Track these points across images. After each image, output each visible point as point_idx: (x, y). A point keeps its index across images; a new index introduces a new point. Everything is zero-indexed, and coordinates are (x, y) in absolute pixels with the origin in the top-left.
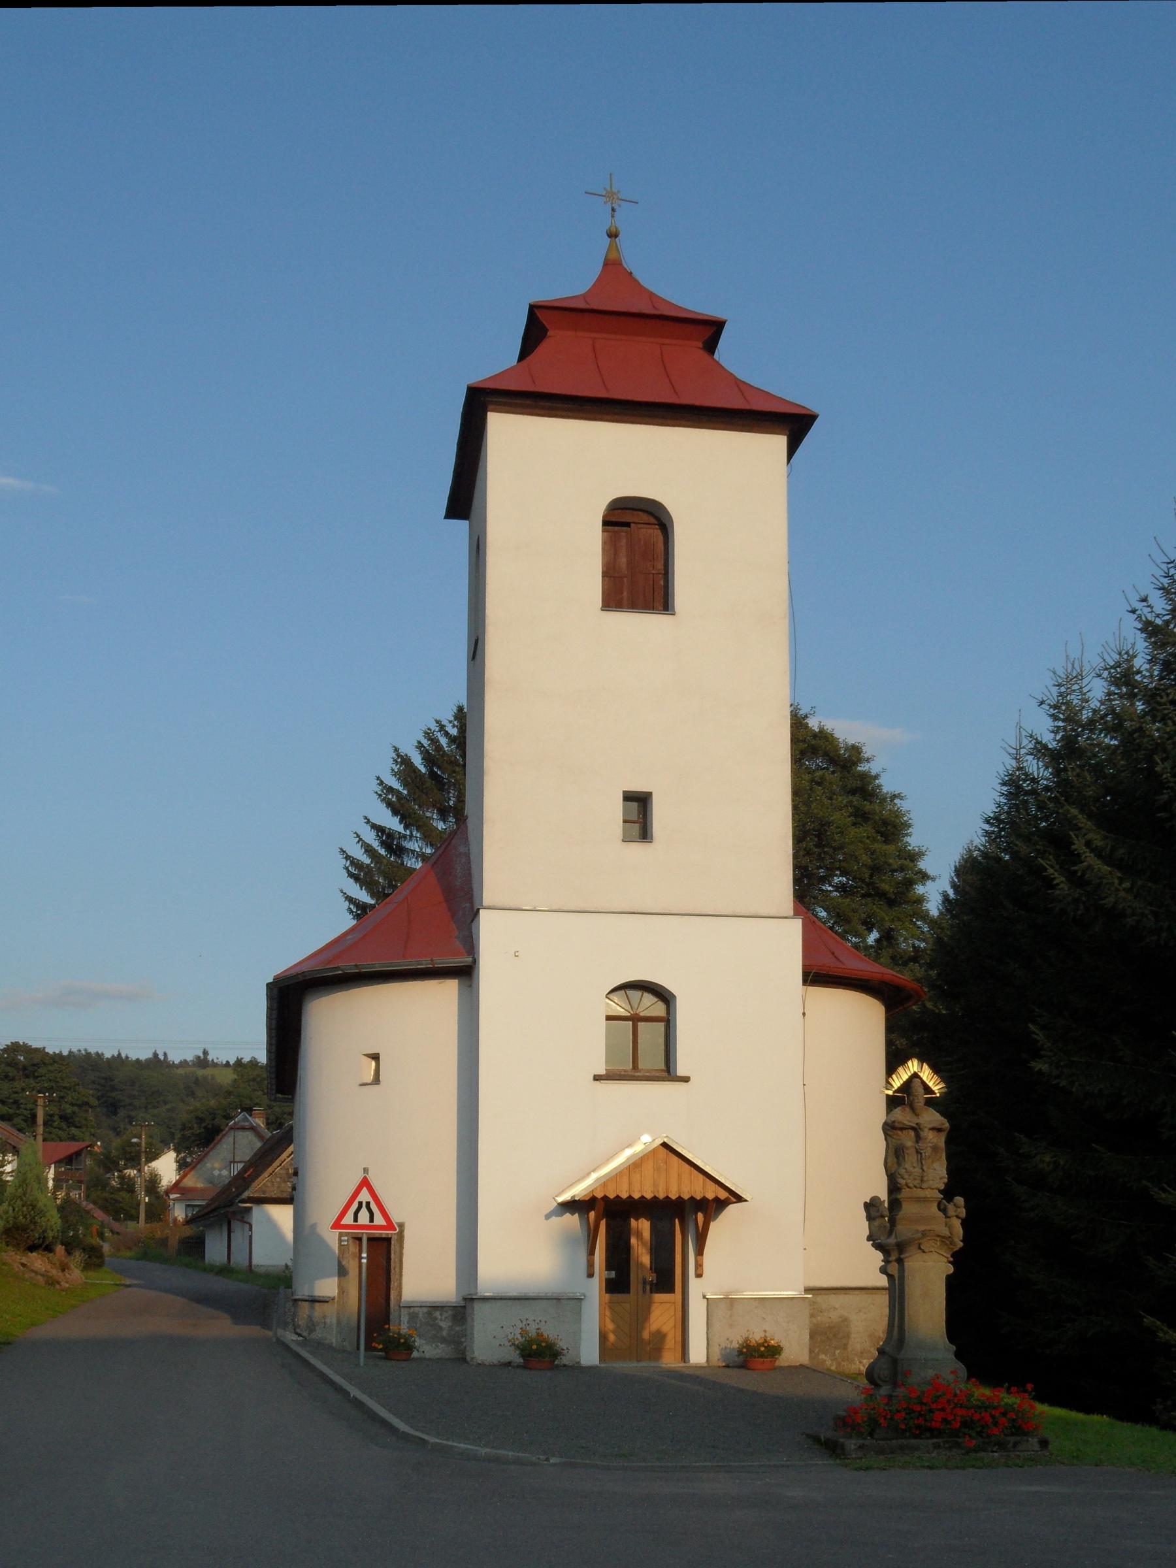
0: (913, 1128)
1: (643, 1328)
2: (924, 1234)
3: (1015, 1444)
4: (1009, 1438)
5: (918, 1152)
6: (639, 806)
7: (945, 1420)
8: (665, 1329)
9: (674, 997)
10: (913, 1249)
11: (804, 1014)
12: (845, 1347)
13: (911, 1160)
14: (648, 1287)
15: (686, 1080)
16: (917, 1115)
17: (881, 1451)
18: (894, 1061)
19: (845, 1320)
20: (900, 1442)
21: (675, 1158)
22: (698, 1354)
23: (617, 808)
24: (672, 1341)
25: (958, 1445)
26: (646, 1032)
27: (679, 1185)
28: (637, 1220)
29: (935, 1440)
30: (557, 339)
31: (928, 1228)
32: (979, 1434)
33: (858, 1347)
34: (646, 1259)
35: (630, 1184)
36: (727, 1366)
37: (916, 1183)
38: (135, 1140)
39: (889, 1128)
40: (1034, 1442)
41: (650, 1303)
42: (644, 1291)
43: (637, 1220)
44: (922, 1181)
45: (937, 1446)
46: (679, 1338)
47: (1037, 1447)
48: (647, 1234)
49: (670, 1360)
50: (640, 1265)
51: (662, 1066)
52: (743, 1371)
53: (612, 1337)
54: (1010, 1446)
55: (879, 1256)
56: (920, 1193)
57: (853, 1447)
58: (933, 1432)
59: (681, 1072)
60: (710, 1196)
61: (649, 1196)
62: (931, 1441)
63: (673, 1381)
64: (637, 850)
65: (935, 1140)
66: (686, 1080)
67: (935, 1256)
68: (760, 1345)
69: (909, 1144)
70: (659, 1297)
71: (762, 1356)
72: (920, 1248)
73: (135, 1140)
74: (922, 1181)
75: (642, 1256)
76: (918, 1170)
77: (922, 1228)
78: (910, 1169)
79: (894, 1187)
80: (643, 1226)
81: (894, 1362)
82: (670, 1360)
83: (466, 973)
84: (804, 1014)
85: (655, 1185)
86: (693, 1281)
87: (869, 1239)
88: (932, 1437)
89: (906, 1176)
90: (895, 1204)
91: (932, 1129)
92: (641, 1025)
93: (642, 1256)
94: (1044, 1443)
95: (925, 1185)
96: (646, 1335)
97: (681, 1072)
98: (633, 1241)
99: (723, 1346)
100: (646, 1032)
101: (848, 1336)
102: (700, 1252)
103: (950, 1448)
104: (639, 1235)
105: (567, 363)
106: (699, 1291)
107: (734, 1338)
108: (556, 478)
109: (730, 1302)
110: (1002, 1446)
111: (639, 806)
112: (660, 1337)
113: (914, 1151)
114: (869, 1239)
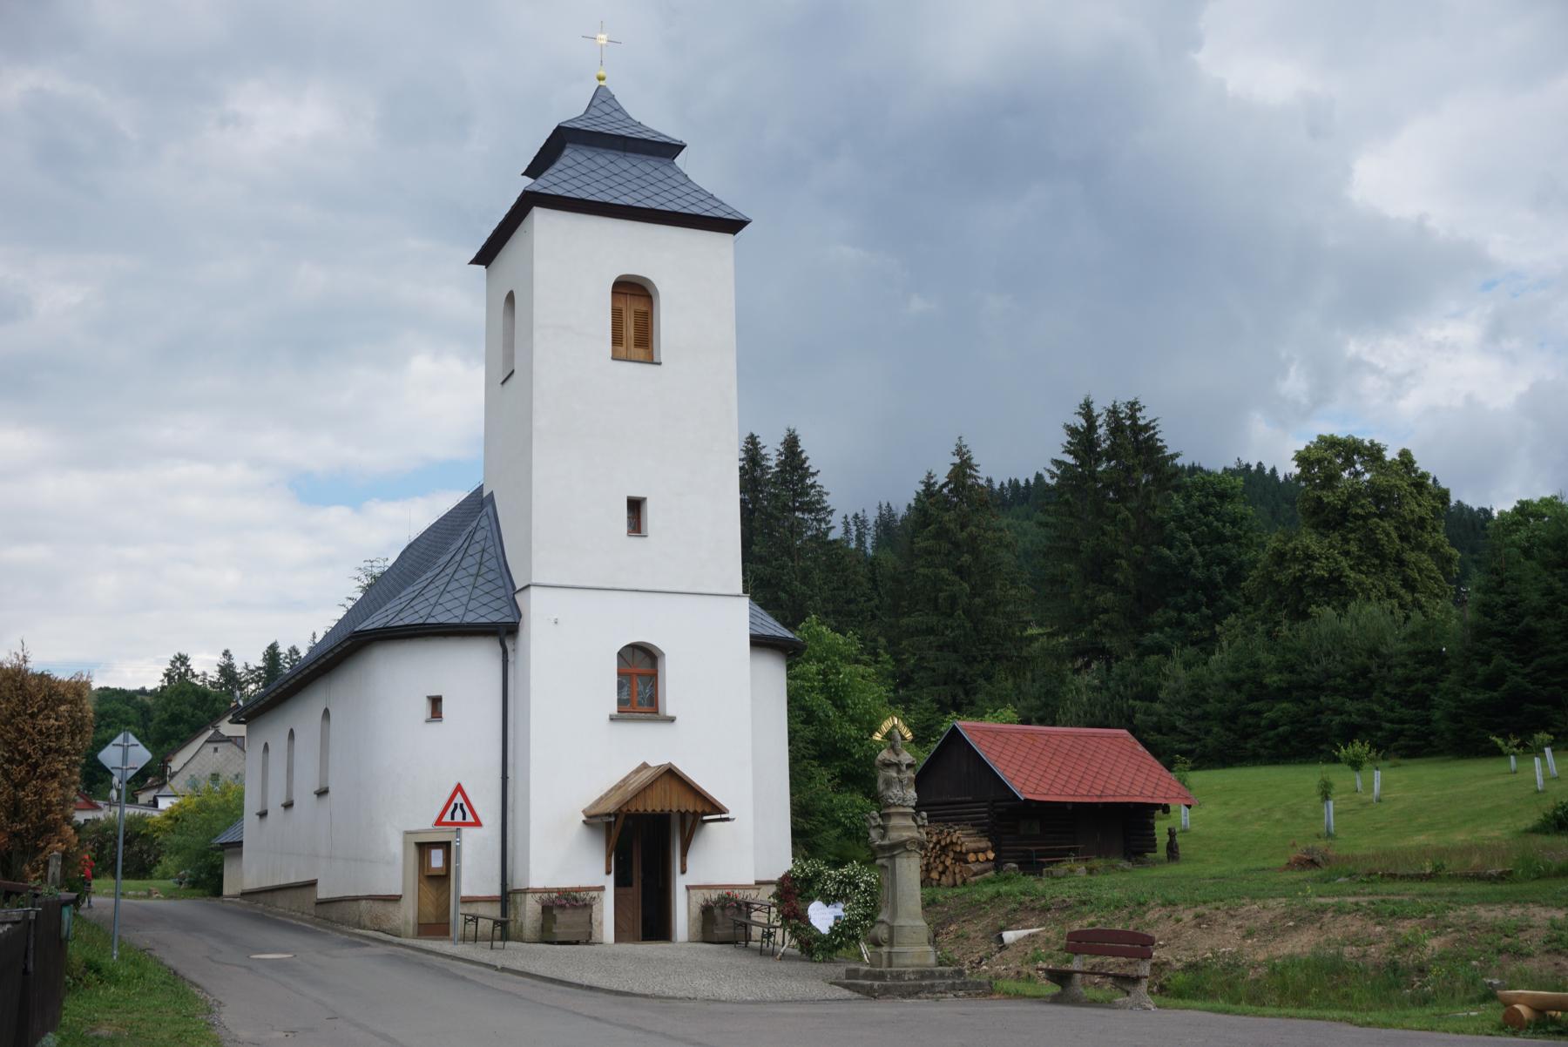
6: (635, 506)
26: (640, 676)
30: (571, 157)
100: (640, 676)
108: (575, 259)
111: (635, 506)
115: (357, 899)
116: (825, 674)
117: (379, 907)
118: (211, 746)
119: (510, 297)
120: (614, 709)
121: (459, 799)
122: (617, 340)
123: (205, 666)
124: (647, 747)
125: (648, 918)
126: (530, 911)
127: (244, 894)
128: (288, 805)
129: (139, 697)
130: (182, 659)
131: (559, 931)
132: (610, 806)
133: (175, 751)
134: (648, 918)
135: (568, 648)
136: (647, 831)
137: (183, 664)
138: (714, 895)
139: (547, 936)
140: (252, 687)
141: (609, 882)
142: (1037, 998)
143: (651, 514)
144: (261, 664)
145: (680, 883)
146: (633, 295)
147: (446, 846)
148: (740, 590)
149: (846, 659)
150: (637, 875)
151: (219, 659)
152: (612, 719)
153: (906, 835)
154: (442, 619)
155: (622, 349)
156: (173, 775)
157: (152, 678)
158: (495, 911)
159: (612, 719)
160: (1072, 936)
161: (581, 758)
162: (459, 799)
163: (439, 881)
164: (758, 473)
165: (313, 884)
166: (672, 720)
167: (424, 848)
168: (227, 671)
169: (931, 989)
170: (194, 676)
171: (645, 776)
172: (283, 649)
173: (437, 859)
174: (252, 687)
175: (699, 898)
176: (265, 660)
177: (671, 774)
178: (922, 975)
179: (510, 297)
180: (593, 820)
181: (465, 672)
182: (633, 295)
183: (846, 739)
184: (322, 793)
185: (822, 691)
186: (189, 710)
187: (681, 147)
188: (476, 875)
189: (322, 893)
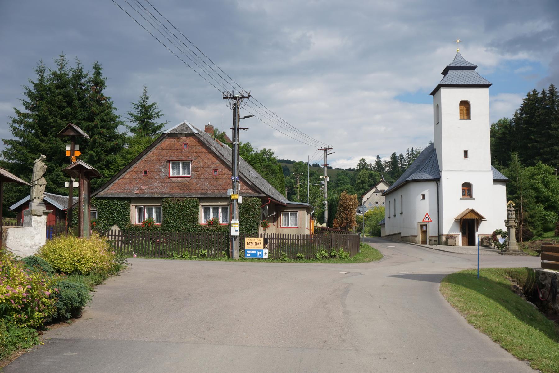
6: (466, 152)
13: (510, 215)
18: (508, 201)
23: (462, 153)
24: (252, 252)
26: (467, 190)
30: (450, 72)
38: (321, 177)
39: (508, 210)
51: (486, 90)
53: (530, 290)
64: (466, 160)
73: (321, 177)
79: (508, 218)
83: (437, 180)
90: (508, 221)
100: (467, 190)
105: (454, 77)
108: (451, 98)
111: (466, 152)
115: (409, 236)
116: (543, 178)
117: (413, 238)
118: (375, 194)
119: (438, 105)
120: (461, 196)
121: (427, 216)
122: (461, 115)
123: (371, 161)
124: (468, 205)
125: (471, 242)
126: (444, 239)
127: (386, 236)
128: (395, 216)
129: (349, 172)
130: (363, 160)
131: (449, 243)
132: (460, 218)
133: (364, 194)
134: (470, 239)
135: (451, 185)
136: (469, 224)
137: (364, 162)
138: (484, 236)
139: (446, 244)
140: (388, 168)
141: (461, 234)
142: (533, 256)
143: (469, 154)
144: (390, 160)
145: (477, 234)
146: (465, 104)
147: (426, 225)
148: (490, 169)
149: (549, 173)
150: (467, 232)
151: (375, 159)
152: (461, 199)
153: (512, 224)
154: (424, 178)
155: (462, 117)
156: (364, 203)
157: (354, 164)
158: (437, 239)
159: (461, 199)
160: (29, 194)
161: (454, 207)
162: (427, 216)
163: (424, 233)
164: (554, 98)
165: (400, 233)
166: (474, 199)
167: (422, 226)
168: (378, 163)
169: (515, 254)
170: (368, 166)
171: (468, 211)
172: (398, 155)
173: (424, 228)
174: (388, 168)
175: (480, 237)
176: (391, 159)
177: (473, 211)
178: (514, 251)
179: (438, 105)
180: (456, 221)
181: (428, 190)
182: (465, 104)
183: (549, 196)
184: (402, 213)
185: (542, 183)
186: (367, 179)
187: (476, 67)
188: (432, 231)
189: (402, 235)
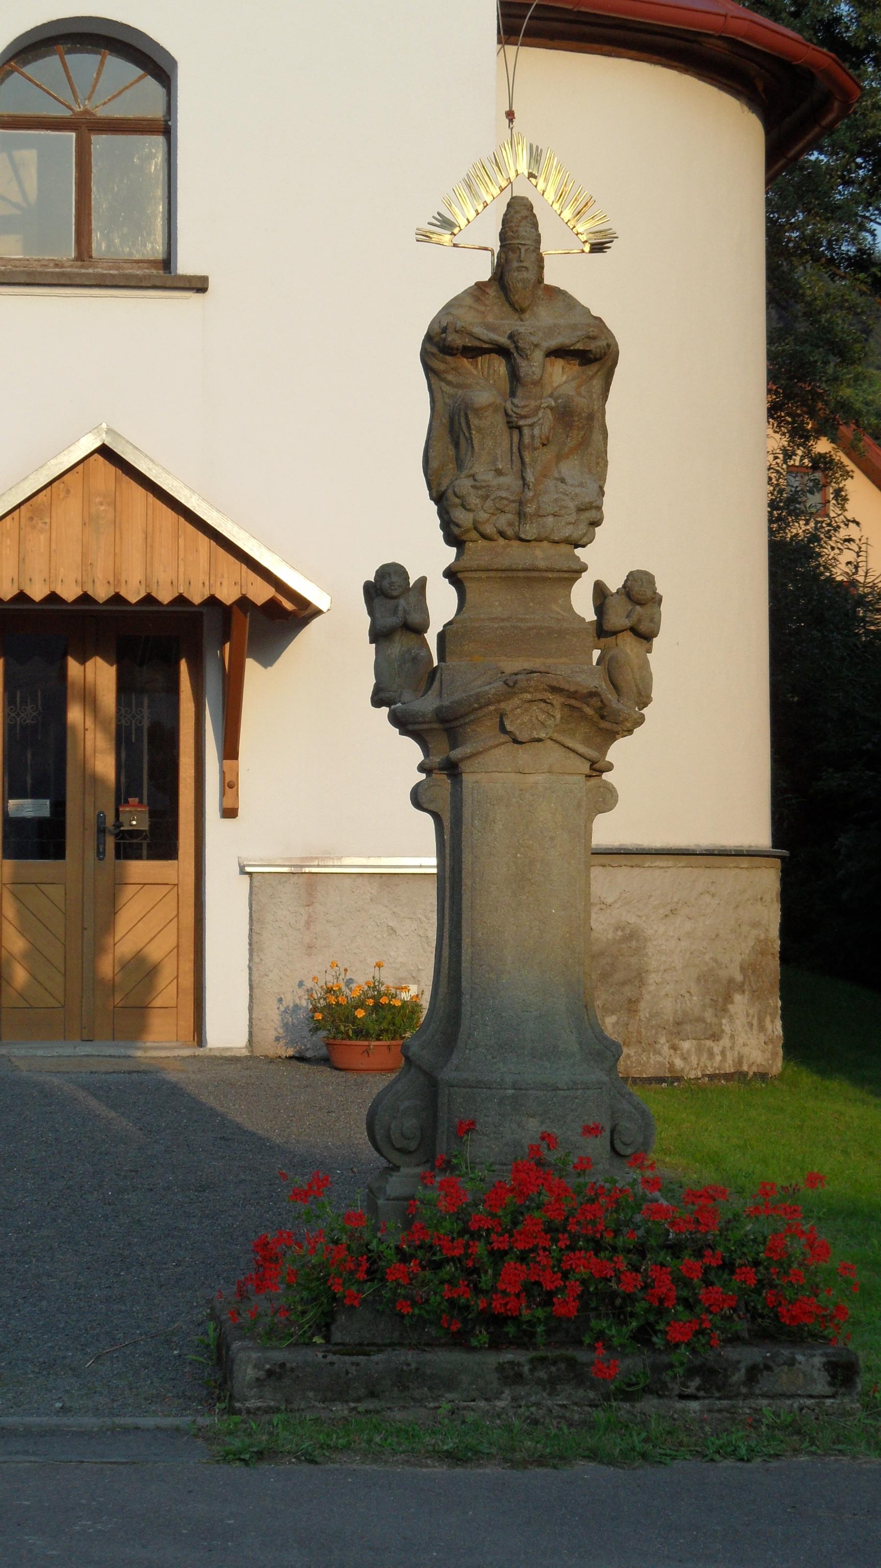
0: (502, 351)
1: (98, 949)
2: (511, 686)
3: (753, 1373)
4: (732, 1353)
5: (513, 426)
7: (530, 1289)
8: (155, 953)
9: (173, 63)
10: (484, 732)
11: (510, 115)
12: (632, 1006)
14: (110, 842)
15: (199, 285)
16: (519, 310)
17: (337, 1390)
19: (632, 937)
20: (408, 1357)
21: (139, 492)
22: (228, 1026)
24: (168, 991)
25: (576, 1373)
27: (148, 565)
28: (83, 661)
29: (508, 1356)
31: (537, 663)
32: (643, 1336)
33: (668, 1008)
34: (105, 765)
35: (22, 560)
36: (300, 1058)
37: (502, 521)
40: (811, 1363)
41: (118, 883)
42: (100, 854)
43: (83, 661)
44: (521, 515)
45: (511, 1376)
46: (188, 981)
47: (821, 1386)
48: (108, 697)
49: (161, 1043)
50: (93, 780)
52: (324, 1074)
54: (738, 1376)
55: (411, 752)
56: (516, 555)
57: (251, 1373)
58: (501, 1329)
59: (185, 266)
60: (228, 595)
61: (69, 593)
62: (492, 1359)
63: (93, 1103)
65: (569, 390)
66: (199, 285)
67: (552, 755)
68: (360, 1004)
69: (483, 397)
70: (139, 869)
71: (361, 1033)
72: (503, 729)
74: (521, 515)
75: (96, 752)
76: (510, 480)
77: (512, 665)
78: (486, 476)
80: (98, 676)
81: (431, 1088)
82: (161, 1043)
84: (510, 115)
85: (86, 564)
86: (215, 824)
87: (378, 700)
88: (495, 1345)
89: (474, 500)
91: (559, 353)
92: (99, 142)
93: (96, 752)
94: (843, 1373)
95: (530, 530)
96: (107, 967)
97: (185, 266)
98: (75, 714)
99: (289, 1001)
101: (639, 978)
102: (230, 750)
103: (552, 1385)
104: (89, 699)
106: (231, 850)
107: (302, 976)
109: (308, 883)
110: (711, 1378)
112: (143, 972)
113: (500, 420)
114: (378, 700)
